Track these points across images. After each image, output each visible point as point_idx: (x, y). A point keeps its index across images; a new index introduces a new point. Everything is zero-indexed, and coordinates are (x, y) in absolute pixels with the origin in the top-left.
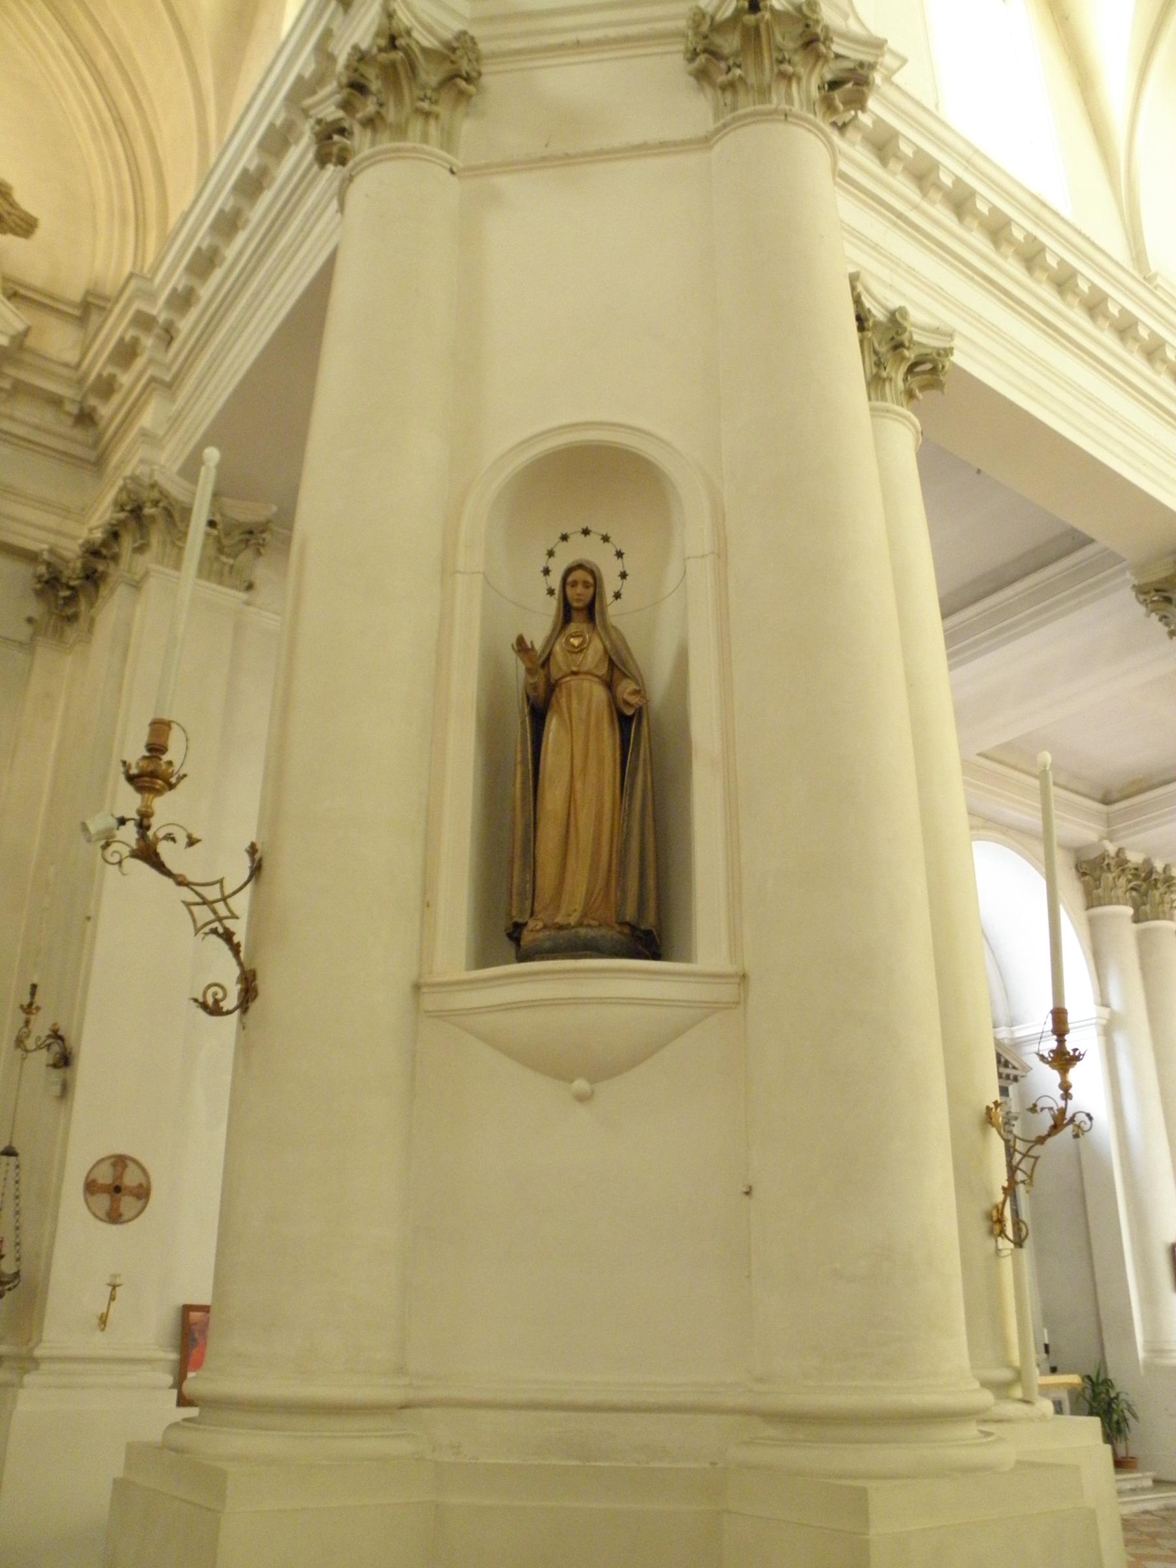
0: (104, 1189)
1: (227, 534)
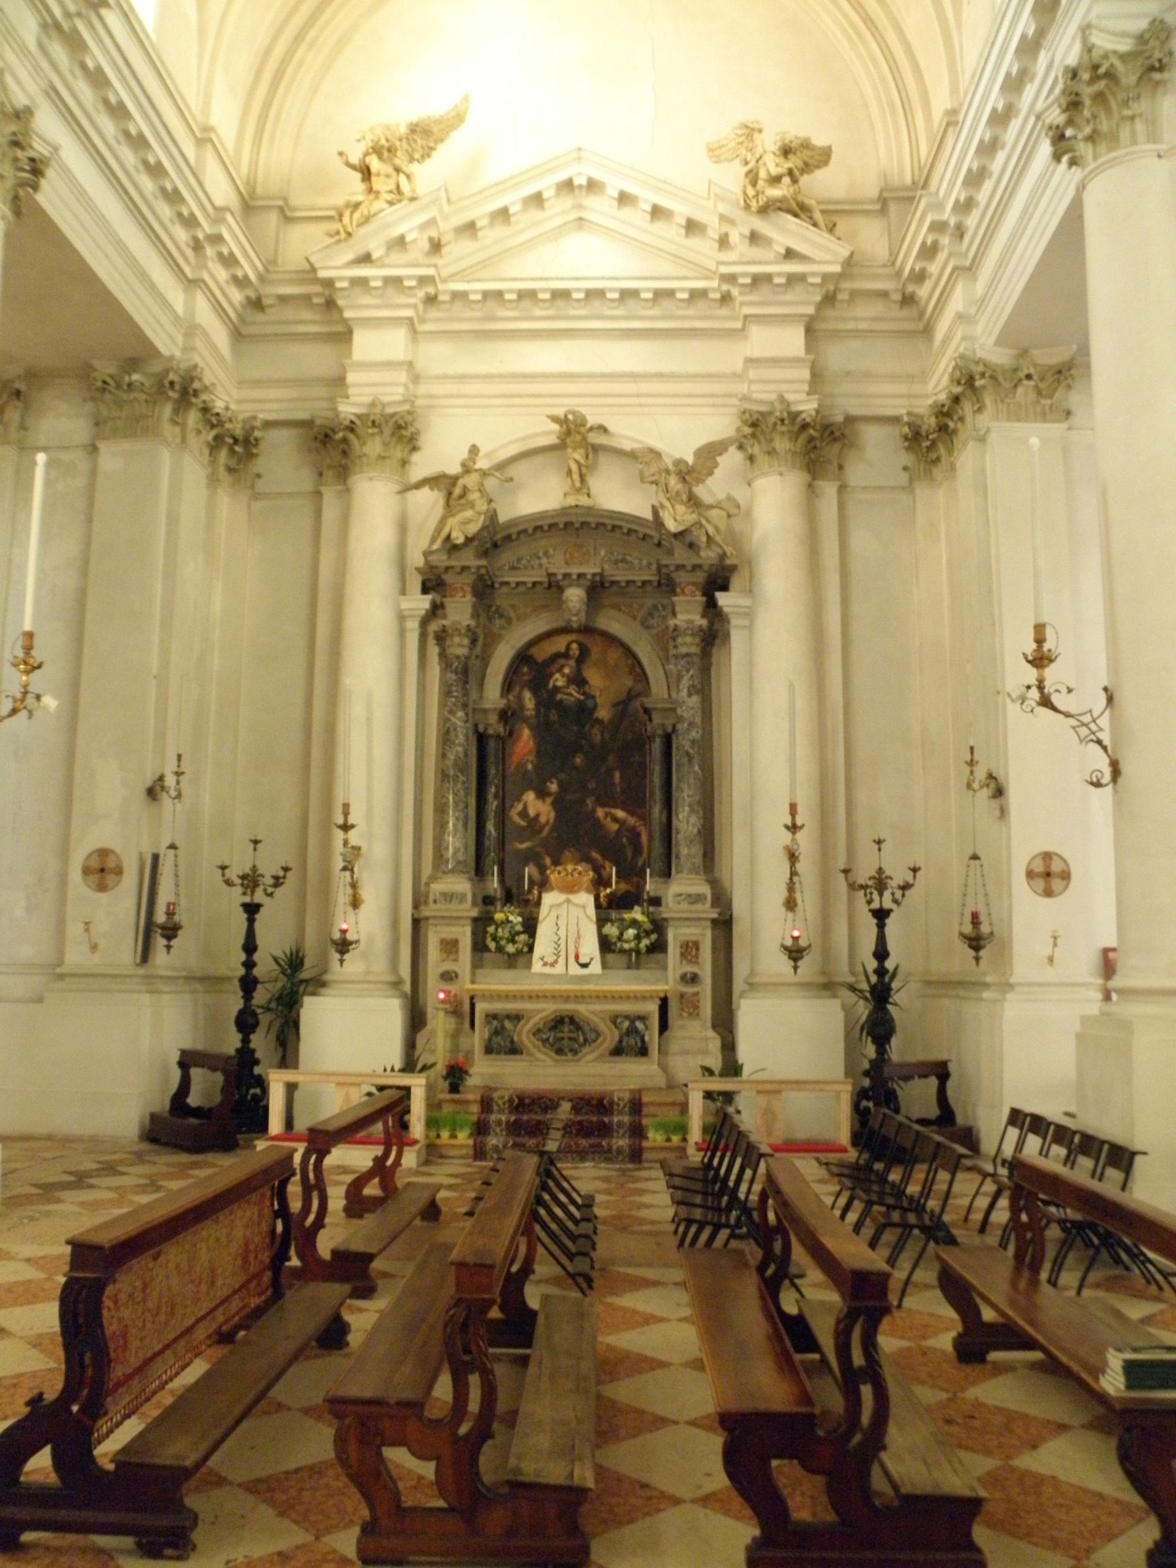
0: (1039, 875)
1: (1042, 379)
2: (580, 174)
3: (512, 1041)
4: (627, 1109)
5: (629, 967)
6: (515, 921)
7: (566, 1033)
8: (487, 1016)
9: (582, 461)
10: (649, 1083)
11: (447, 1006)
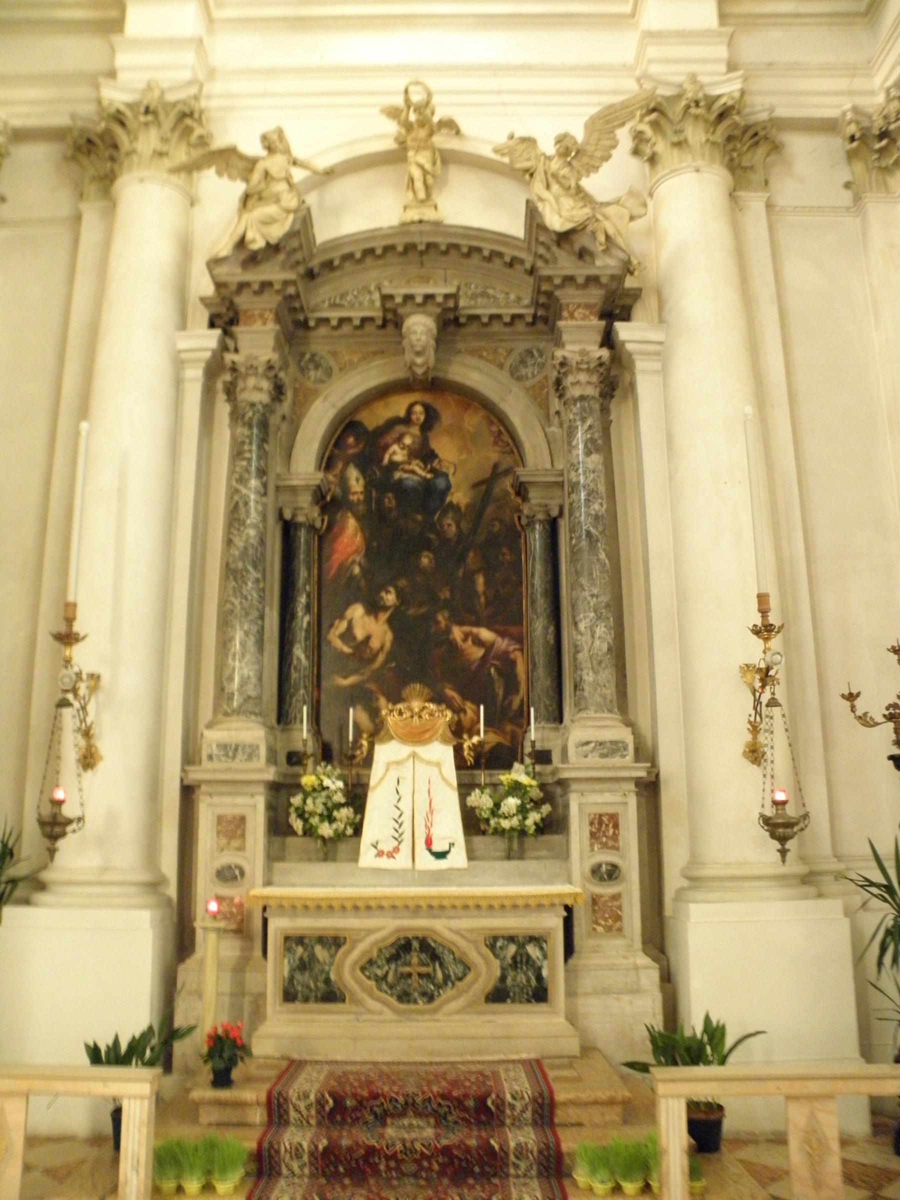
3: (328, 981)
4: (528, 1115)
5: (509, 857)
6: (333, 787)
7: (415, 965)
8: (287, 939)
9: (428, 166)
10: (552, 1048)
11: (222, 924)
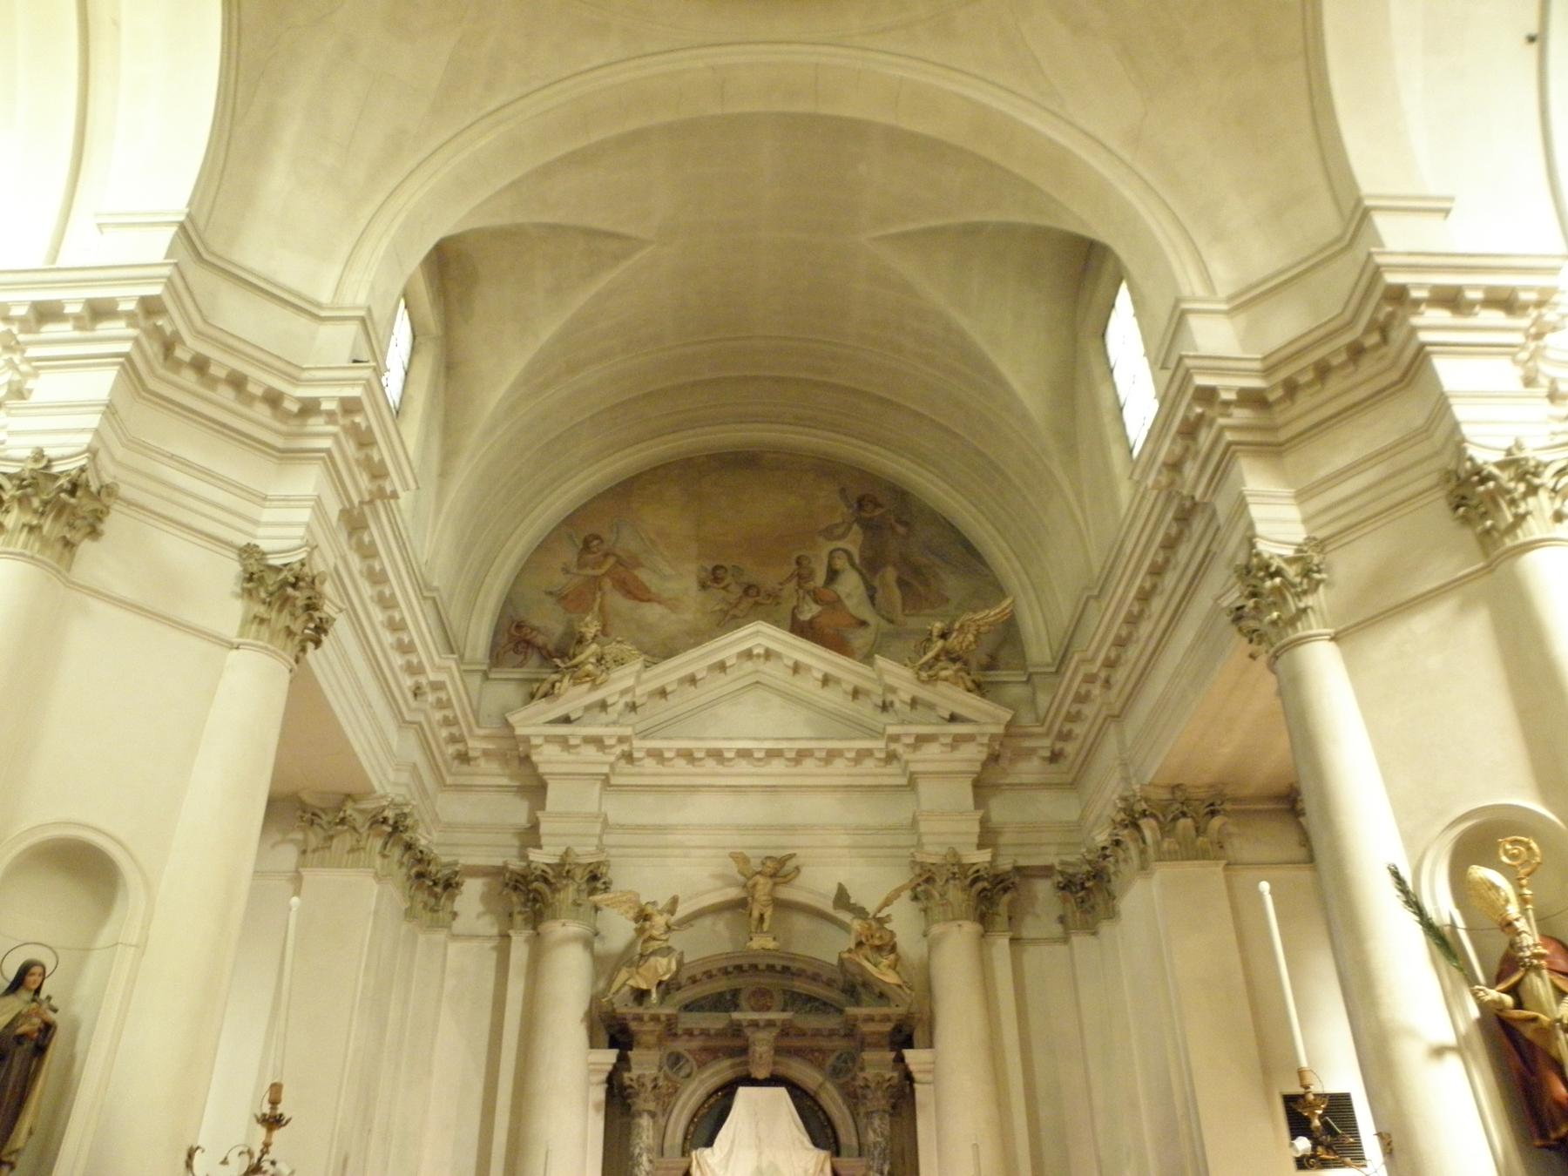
2: (759, 645)
